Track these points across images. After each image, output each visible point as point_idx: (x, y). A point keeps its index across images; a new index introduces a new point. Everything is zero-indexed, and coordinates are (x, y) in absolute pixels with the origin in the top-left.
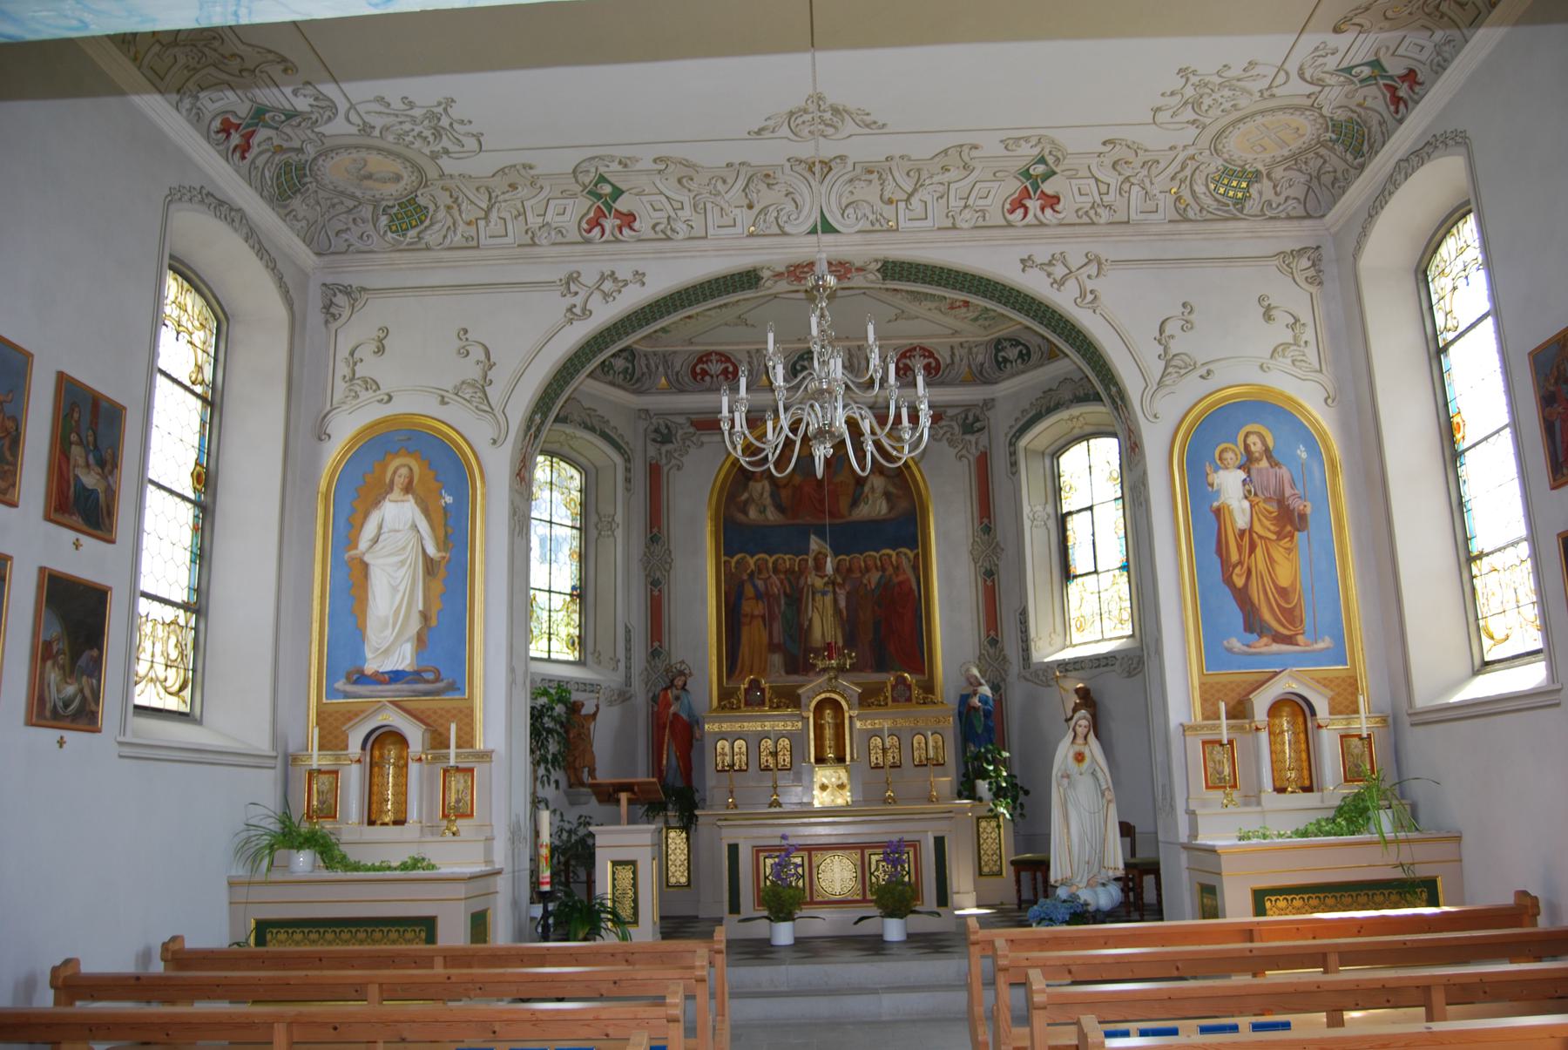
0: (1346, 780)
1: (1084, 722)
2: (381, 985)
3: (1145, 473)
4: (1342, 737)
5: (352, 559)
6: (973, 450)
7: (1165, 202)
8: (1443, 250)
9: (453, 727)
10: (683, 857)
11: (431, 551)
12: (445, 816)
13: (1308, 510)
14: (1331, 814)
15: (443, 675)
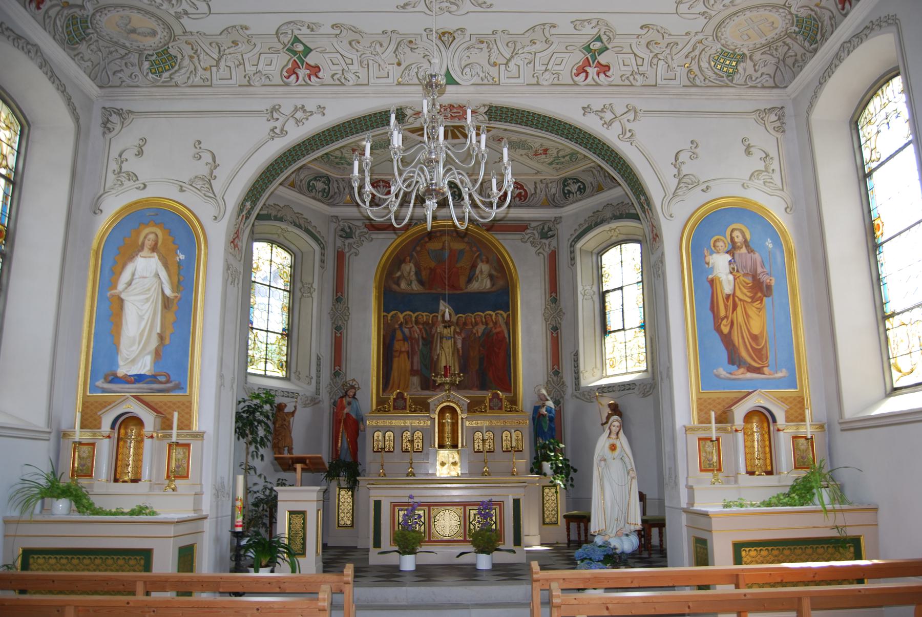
0: (796, 468)
1: (617, 424)
2: (76, 607)
3: (663, 254)
4: (793, 438)
5: (113, 296)
6: (547, 249)
7: (681, 73)
8: (871, 107)
9: (176, 414)
10: (350, 508)
11: (168, 292)
12: (168, 477)
13: (773, 283)
14: (787, 490)
15: (172, 379)
